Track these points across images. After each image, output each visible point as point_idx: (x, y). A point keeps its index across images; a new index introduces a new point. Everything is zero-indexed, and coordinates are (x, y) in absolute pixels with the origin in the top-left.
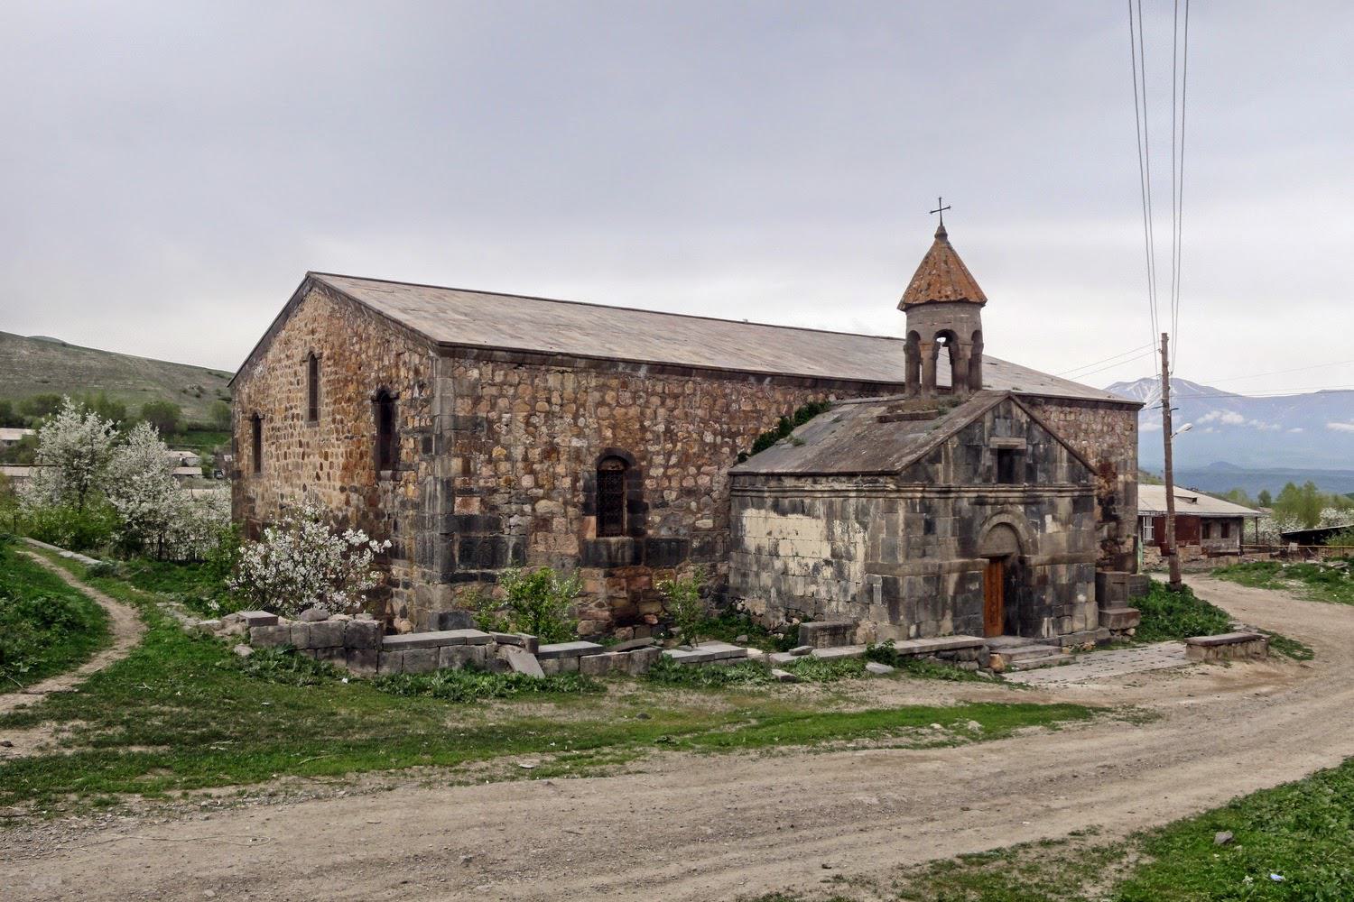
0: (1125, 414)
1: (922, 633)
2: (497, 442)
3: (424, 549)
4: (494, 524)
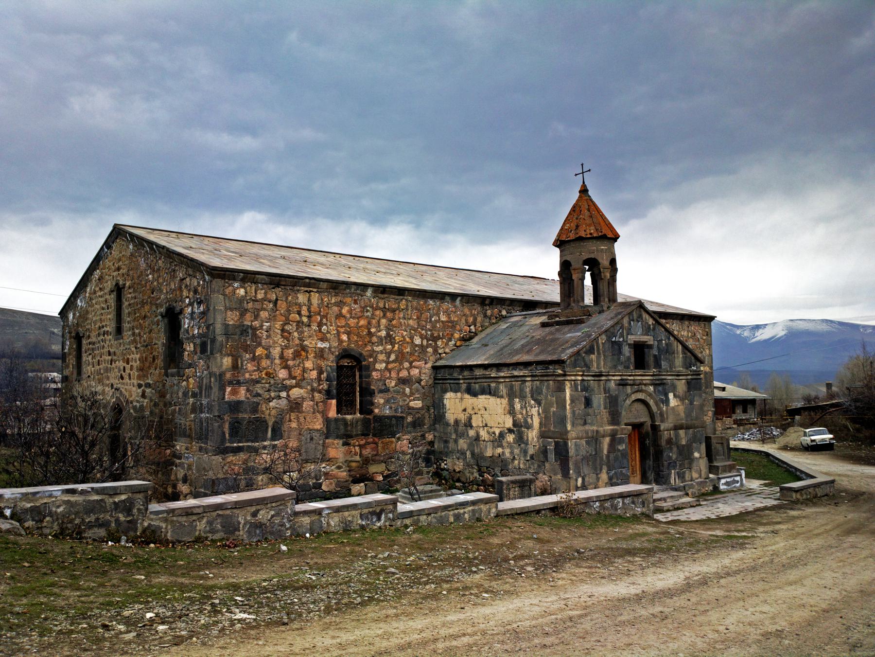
0: (702, 324)
3: (201, 429)
4: (255, 408)
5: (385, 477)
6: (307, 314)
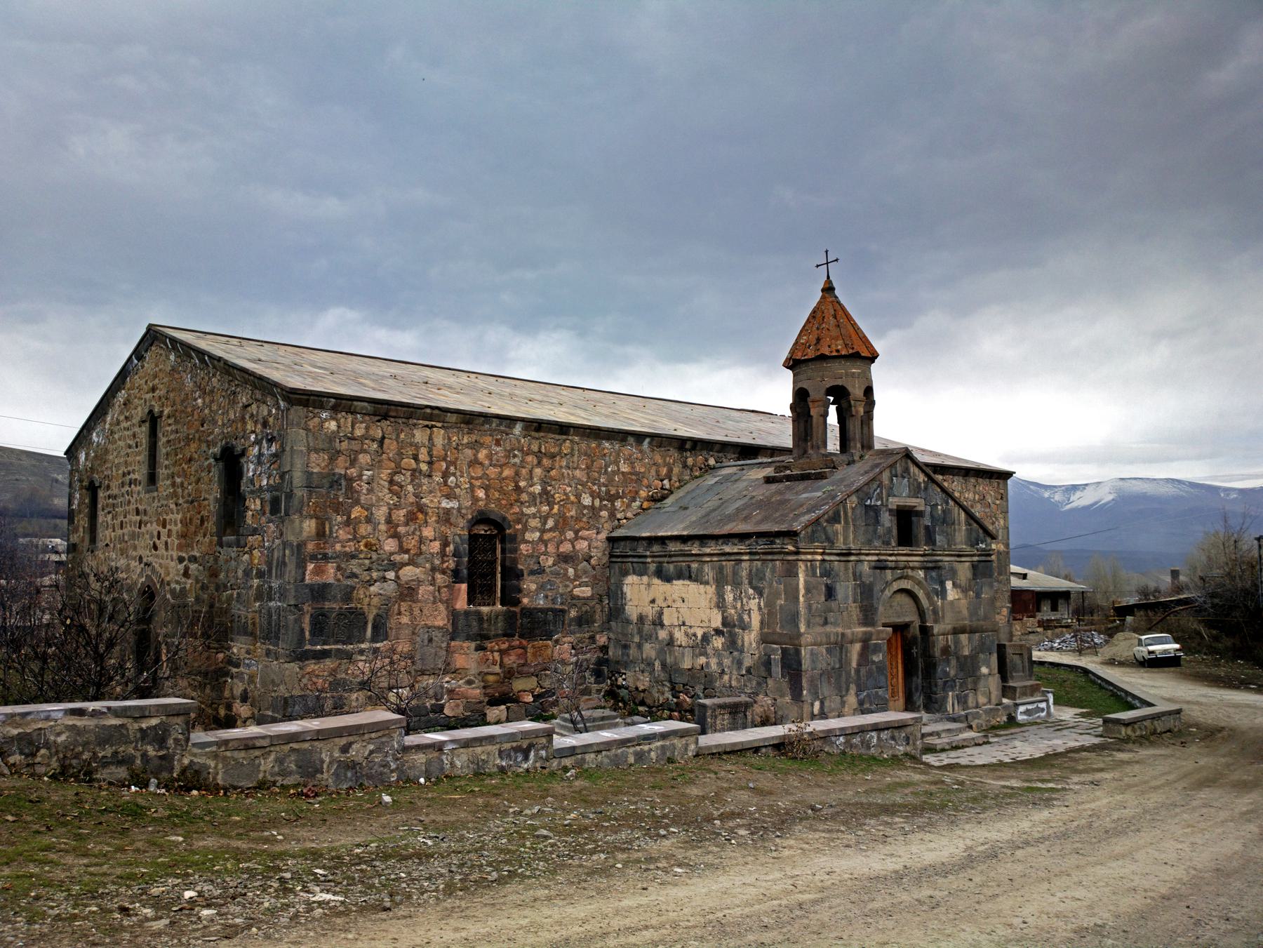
0: (995, 482)
2: (357, 502)
3: (269, 623)
5: (536, 697)
6: (427, 459)
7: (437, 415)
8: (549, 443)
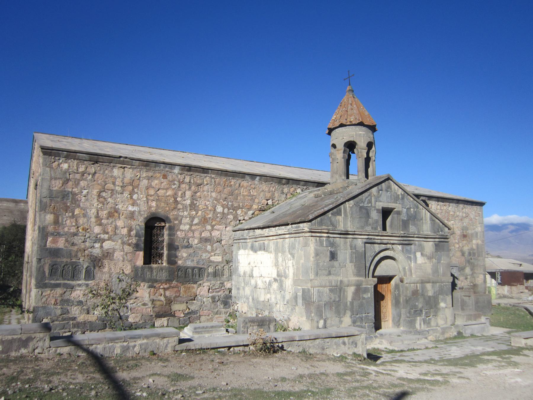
1: (328, 325)
2: (79, 206)
5: (186, 315)
6: (121, 184)
7: (128, 162)
8: (197, 178)
